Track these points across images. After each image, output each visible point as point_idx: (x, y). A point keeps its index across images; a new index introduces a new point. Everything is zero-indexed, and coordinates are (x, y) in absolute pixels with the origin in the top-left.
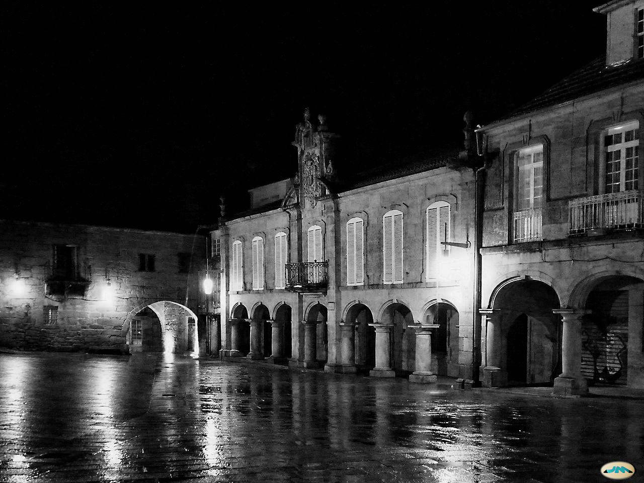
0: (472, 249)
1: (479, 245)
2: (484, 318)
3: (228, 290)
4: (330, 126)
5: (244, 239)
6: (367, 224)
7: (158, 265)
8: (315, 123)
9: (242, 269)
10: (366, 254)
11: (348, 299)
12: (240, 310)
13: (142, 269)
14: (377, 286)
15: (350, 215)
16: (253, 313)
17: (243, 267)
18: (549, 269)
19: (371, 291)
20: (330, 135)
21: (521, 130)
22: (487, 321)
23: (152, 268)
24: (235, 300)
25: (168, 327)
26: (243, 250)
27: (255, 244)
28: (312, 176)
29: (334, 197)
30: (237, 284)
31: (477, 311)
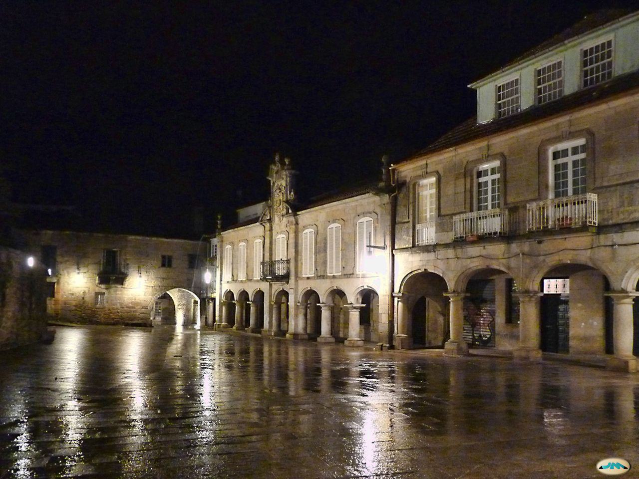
0: (389, 249)
1: (393, 248)
2: (396, 300)
3: (221, 280)
4: (293, 166)
5: (232, 244)
6: (317, 233)
7: (175, 263)
8: (283, 164)
9: (231, 265)
10: (316, 253)
11: (303, 286)
12: (230, 294)
13: (163, 265)
14: (323, 277)
15: (305, 227)
16: (238, 297)
17: (232, 264)
18: (441, 264)
19: (319, 281)
20: (293, 172)
21: (421, 167)
22: (398, 301)
23: (170, 266)
24: (226, 287)
25: (180, 307)
26: (232, 252)
27: (240, 247)
28: (280, 200)
29: (295, 215)
30: (227, 276)
31: (392, 294)
